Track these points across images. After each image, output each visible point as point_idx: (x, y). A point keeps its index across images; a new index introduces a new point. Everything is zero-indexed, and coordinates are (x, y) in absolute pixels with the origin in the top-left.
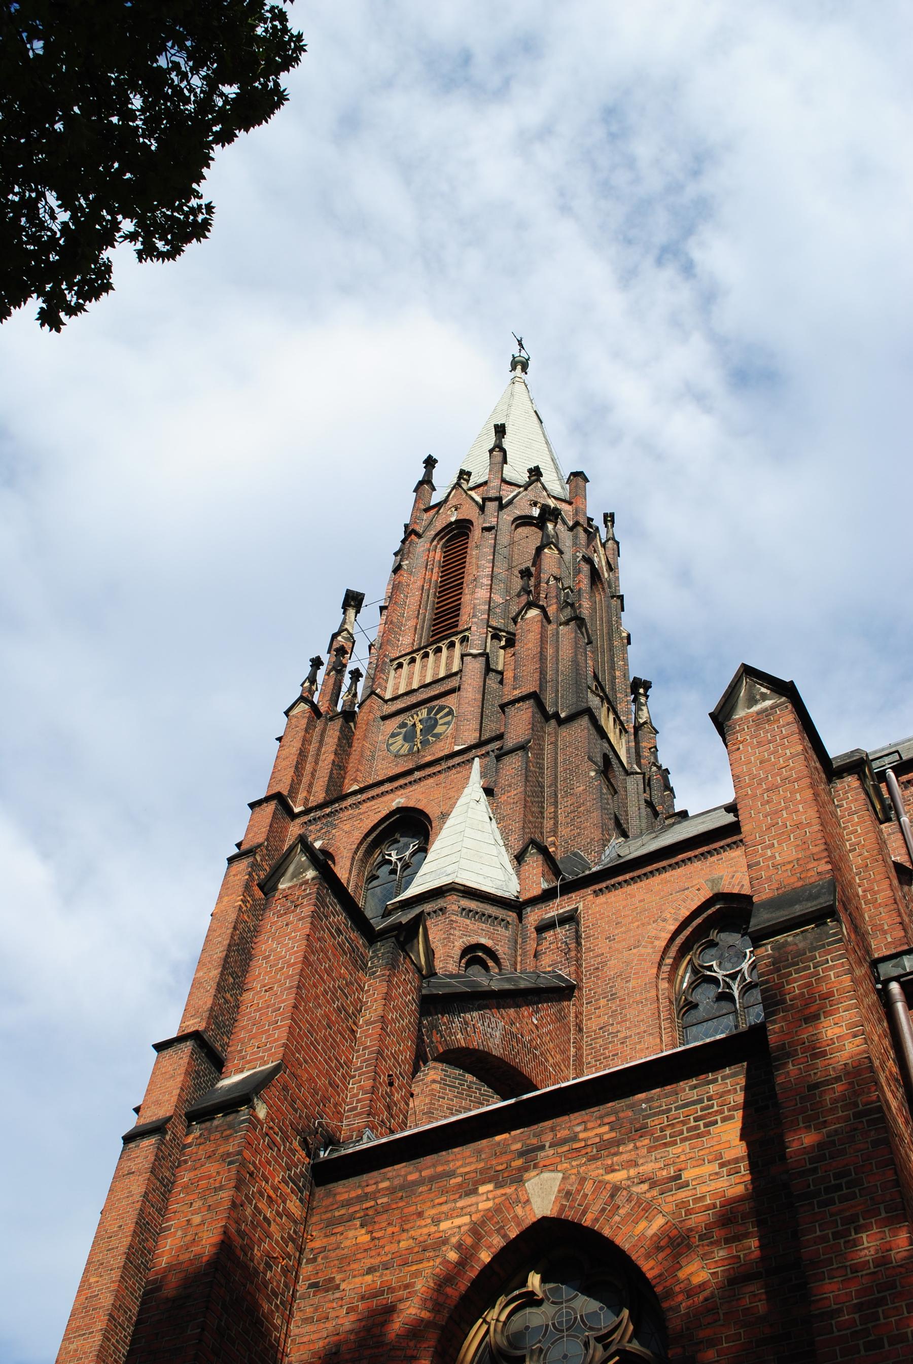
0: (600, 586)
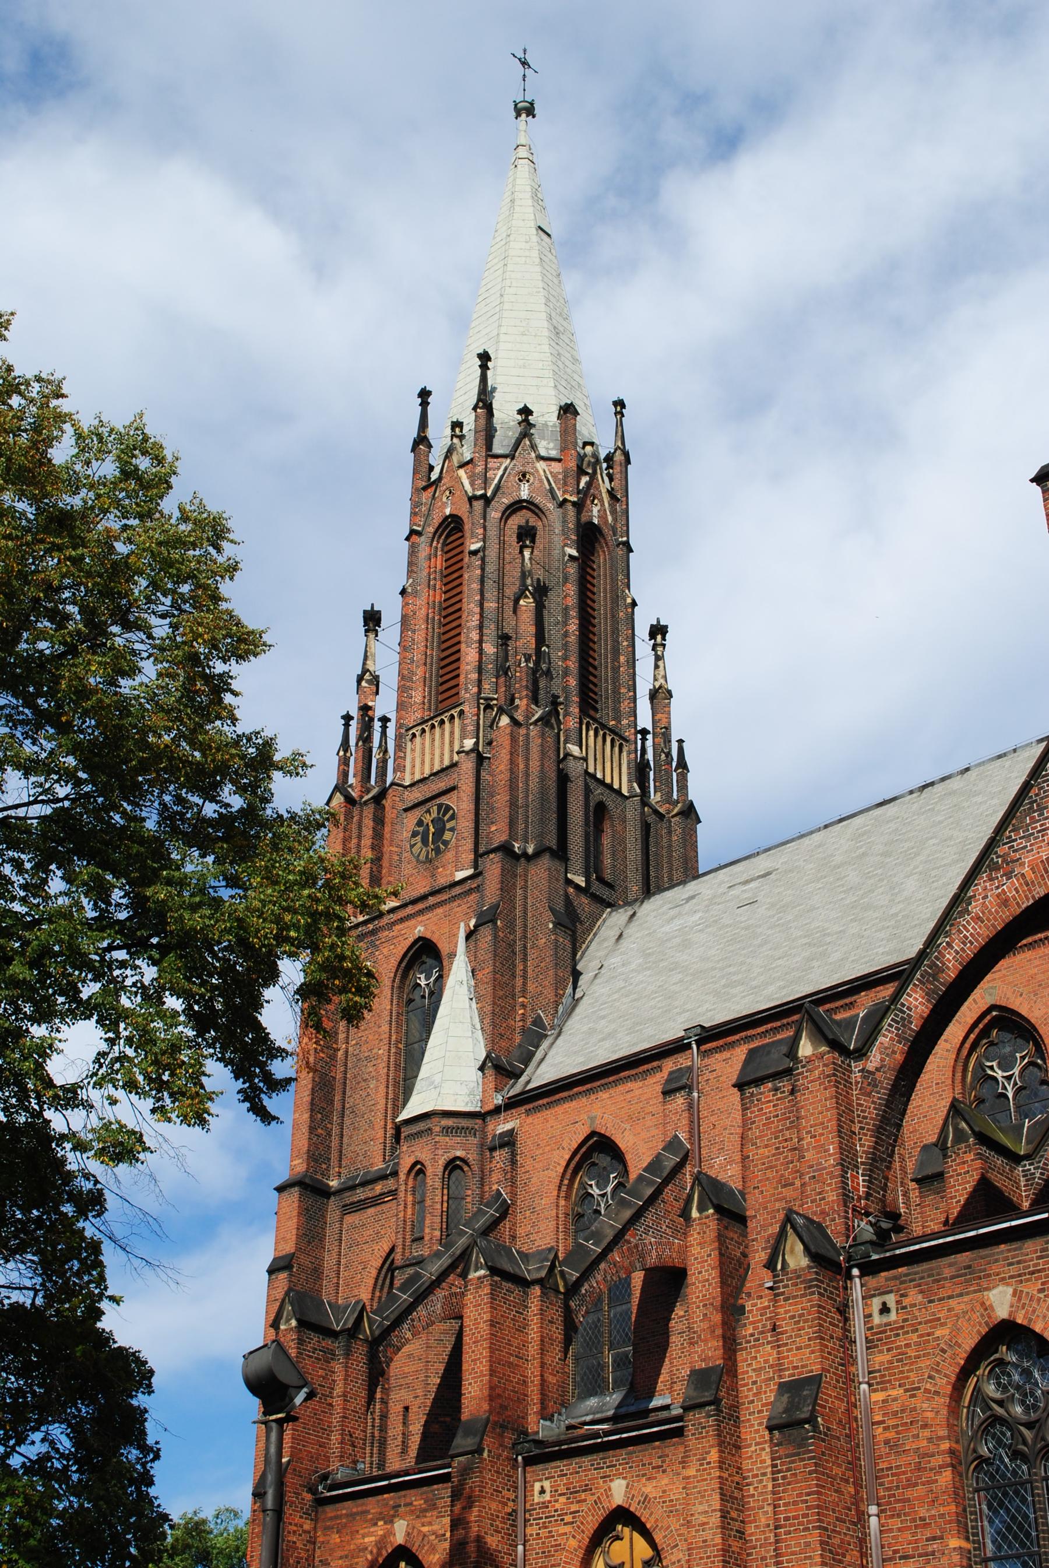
0: (603, 541)
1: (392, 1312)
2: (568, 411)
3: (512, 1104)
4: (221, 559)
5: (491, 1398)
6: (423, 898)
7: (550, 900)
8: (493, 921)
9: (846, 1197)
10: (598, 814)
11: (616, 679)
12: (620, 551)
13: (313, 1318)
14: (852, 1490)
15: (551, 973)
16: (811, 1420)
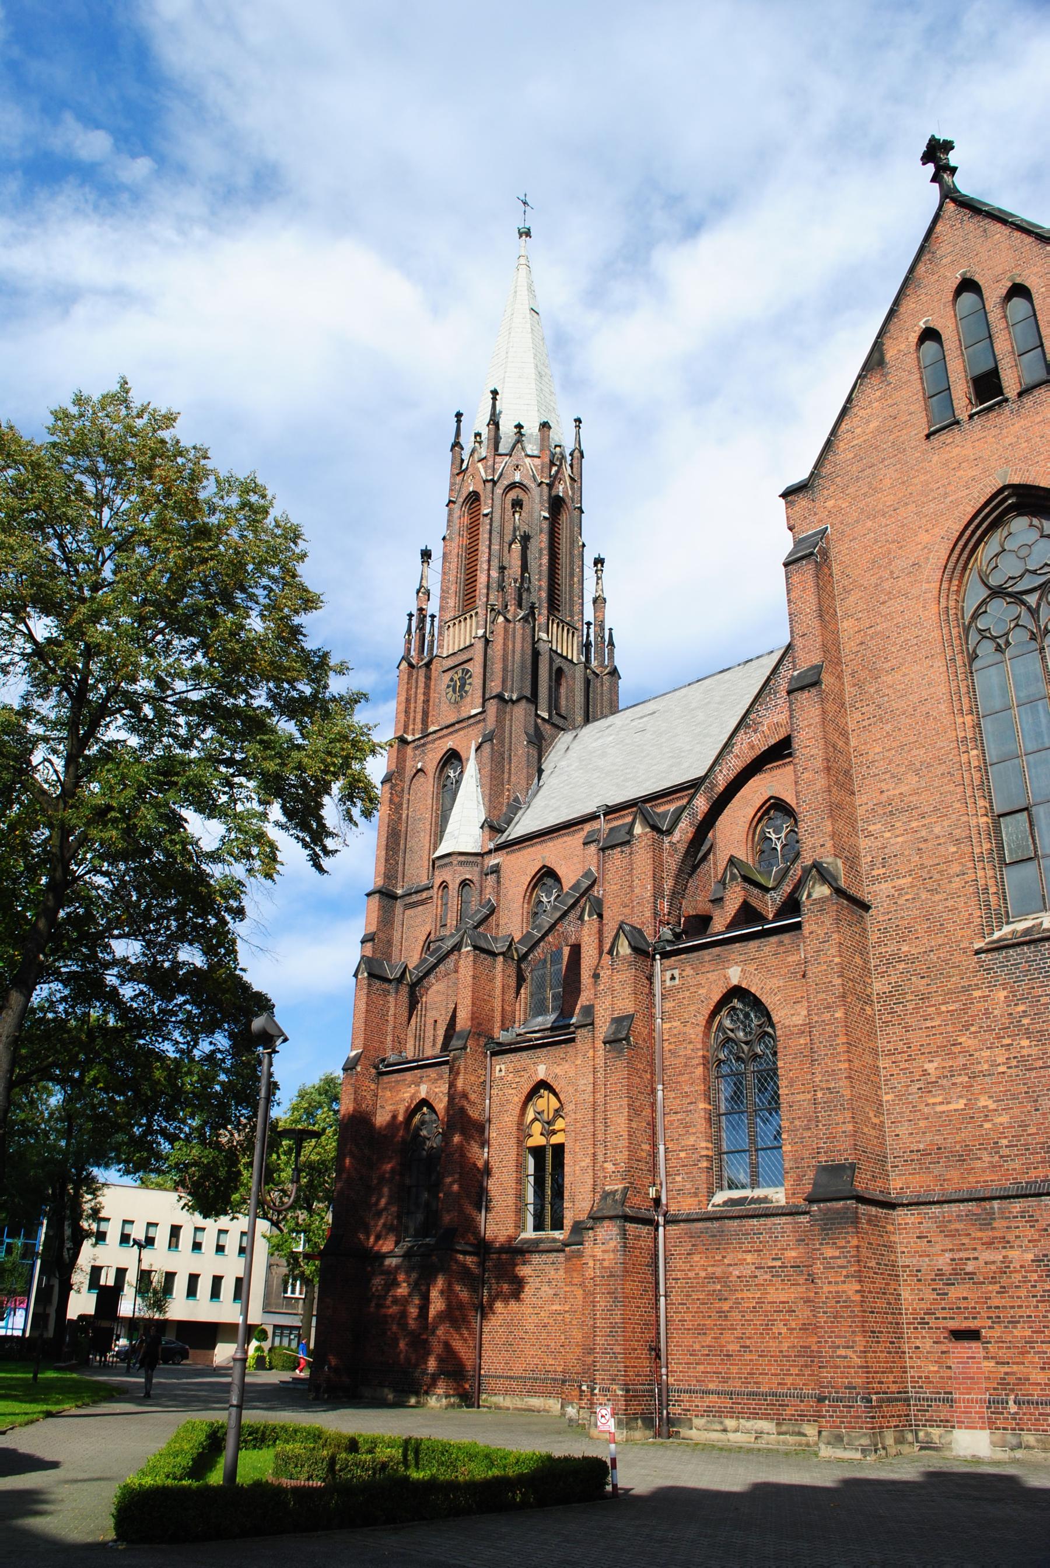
1: (424, 968)
2: (545, 426)
3: (499, 848)
4: (297, 551)
5: (472, 1019)
6: (453, 725)
7: (525, 728)
8: (491, 740)
9: (656, 914)
10: (558, 675)
11: (571, 592)
12: (576, 513)
13: (377, 972)
14: (649, 1077)
15: (525, 771)
16: (627, 1039)
